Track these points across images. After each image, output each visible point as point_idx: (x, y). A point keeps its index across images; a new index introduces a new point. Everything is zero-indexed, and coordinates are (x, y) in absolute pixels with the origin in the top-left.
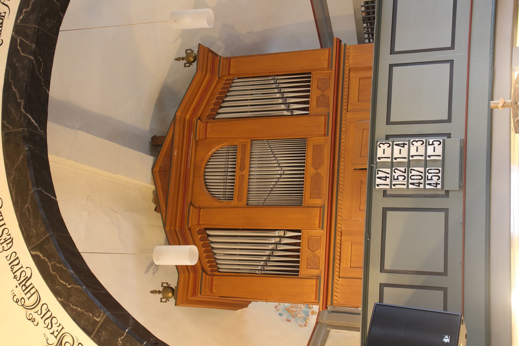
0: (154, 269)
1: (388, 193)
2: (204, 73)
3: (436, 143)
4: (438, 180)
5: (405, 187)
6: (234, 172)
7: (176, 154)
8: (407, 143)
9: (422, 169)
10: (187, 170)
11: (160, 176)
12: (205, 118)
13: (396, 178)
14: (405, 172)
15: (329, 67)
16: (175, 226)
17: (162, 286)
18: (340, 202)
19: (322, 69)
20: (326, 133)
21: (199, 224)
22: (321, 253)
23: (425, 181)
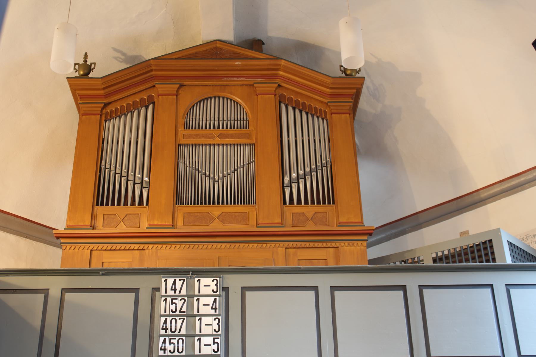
0: (121, 58)
1: (157, 293)
2: (331, 86)
3: (215, 347)
4: (170, 351)
5: (163, 313)
6: (219, 128)
7: (236, 63)
8: (217, 312)
9: (183, 332)
10: (220, 77)
11: (211, 49)
12: (280, 91)
13: (174, 301)
14: (180, 312)
15: (340, 224)
16: (156, 70)
17: (92, 64)
18: (178, 246)
19: (338, 217)
20: (260, 225)
21: (159, 96)
22: (122, 229)
23: (168, 336)
